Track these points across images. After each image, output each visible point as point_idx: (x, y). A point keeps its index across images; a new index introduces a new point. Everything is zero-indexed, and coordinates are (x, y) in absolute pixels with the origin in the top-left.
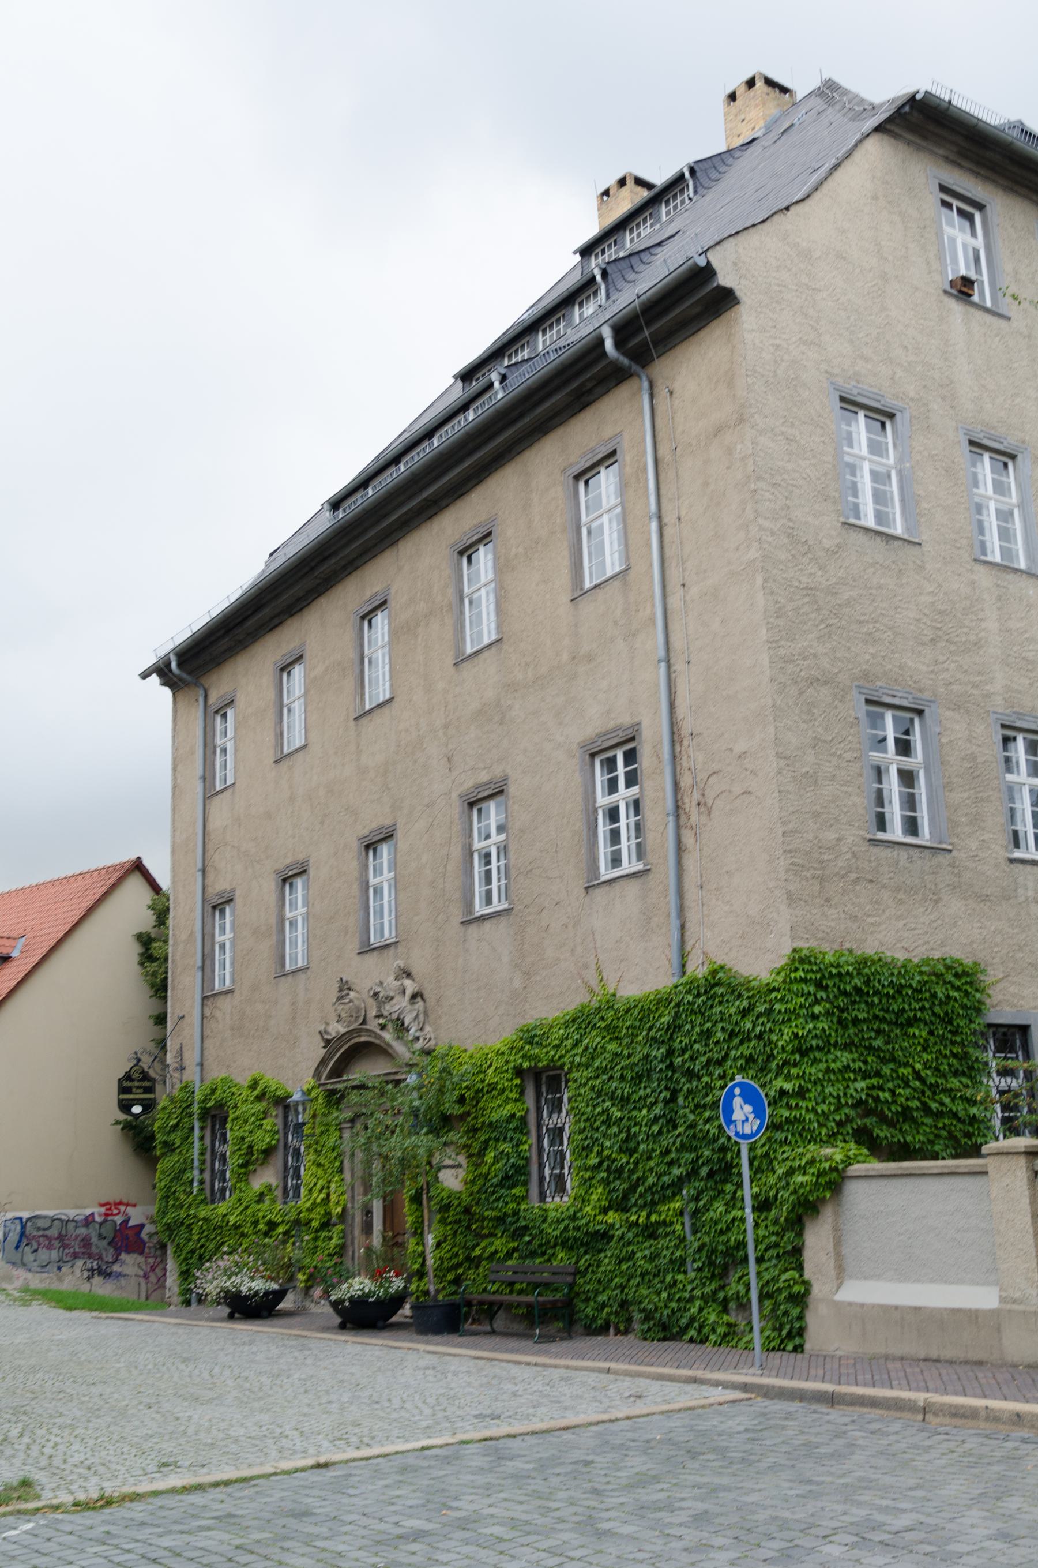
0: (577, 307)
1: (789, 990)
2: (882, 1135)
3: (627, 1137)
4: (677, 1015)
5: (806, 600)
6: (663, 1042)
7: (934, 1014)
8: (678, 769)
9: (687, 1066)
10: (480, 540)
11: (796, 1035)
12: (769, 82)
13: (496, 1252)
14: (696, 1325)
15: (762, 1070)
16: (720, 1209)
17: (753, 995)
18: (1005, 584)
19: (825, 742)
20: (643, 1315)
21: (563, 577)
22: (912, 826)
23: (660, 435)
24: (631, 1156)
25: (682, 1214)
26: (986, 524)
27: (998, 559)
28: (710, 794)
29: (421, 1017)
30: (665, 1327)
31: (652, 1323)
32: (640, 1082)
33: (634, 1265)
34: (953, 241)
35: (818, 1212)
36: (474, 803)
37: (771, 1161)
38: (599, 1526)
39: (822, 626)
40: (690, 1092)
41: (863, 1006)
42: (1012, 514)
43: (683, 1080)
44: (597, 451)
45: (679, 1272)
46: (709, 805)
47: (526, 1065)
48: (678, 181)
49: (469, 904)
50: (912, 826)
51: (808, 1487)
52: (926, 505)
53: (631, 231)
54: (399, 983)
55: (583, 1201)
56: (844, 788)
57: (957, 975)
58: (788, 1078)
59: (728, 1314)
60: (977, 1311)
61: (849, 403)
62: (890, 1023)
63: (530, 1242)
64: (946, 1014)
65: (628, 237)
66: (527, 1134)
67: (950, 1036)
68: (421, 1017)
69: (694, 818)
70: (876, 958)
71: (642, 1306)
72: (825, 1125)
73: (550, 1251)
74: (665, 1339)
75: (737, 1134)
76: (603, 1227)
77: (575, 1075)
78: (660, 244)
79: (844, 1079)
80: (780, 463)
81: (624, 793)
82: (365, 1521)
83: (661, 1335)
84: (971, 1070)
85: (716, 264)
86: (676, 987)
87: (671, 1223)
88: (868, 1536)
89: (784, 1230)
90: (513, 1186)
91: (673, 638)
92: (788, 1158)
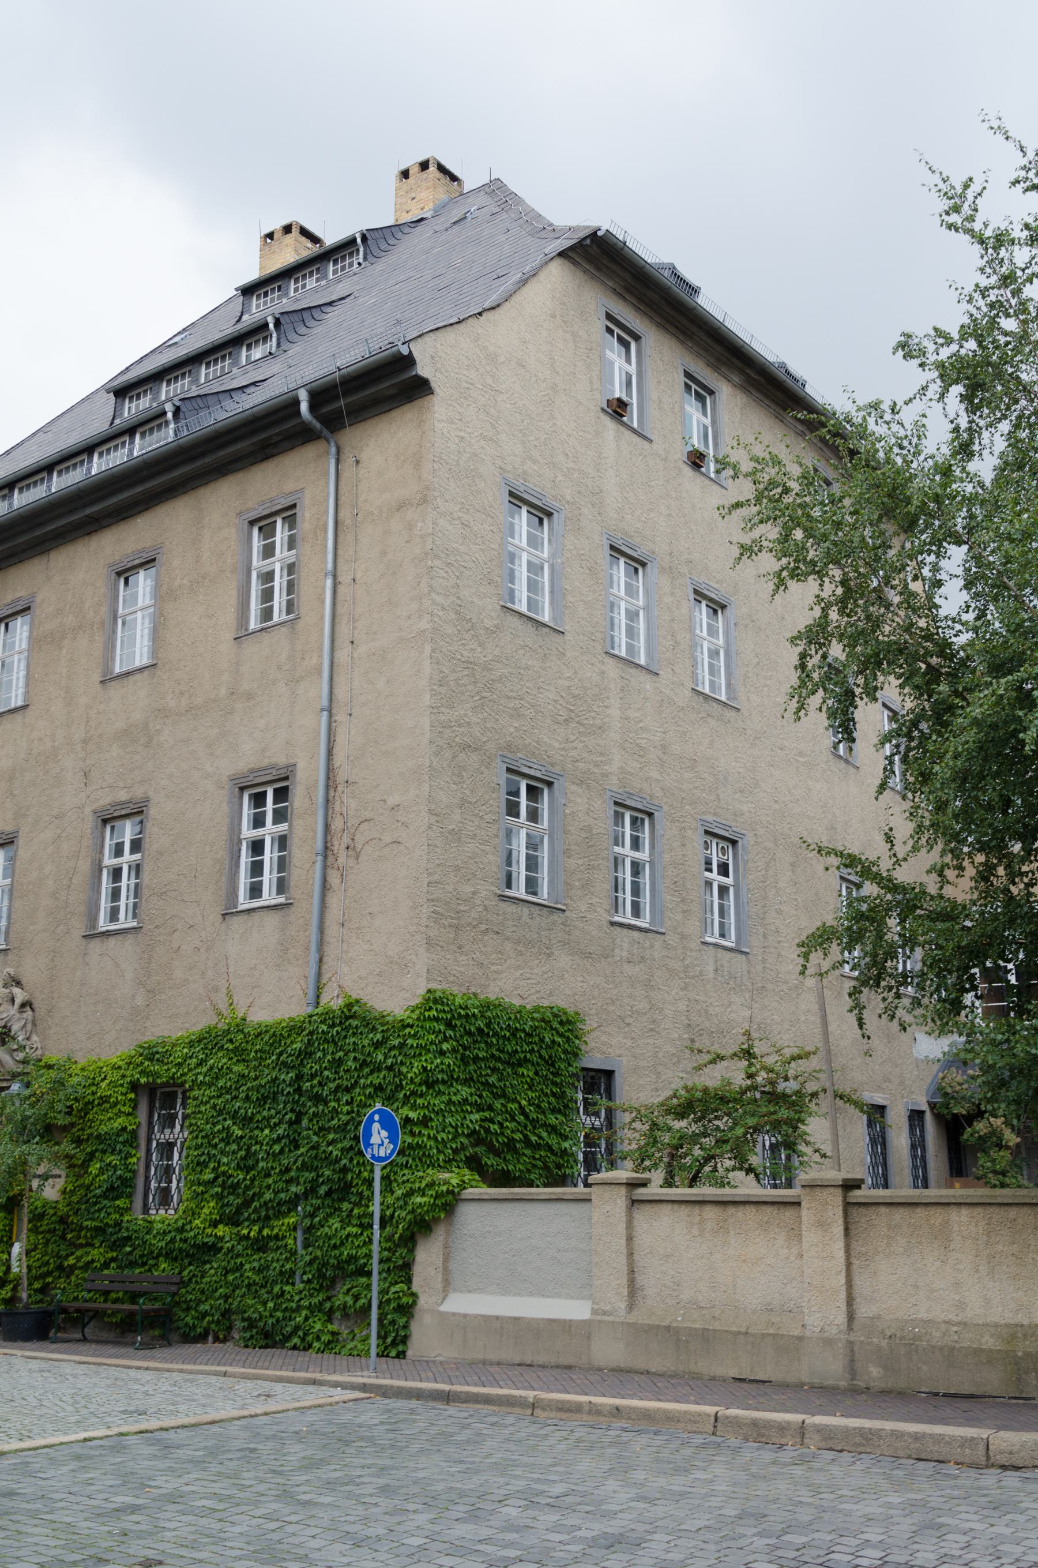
0: (244, 349)
1: (422, 1027)
2: (489, 1163)
3: (246, 1156)
4: (310, 1043)
5: (466, 673)
6: (294, 1066)
7: (541, 1056)
8: (330, 813)
9: (315, 1090)
10: (141, 565)
11: (425, 1069)
12: (441, 168)
13: (93, 1261)
14: (301, 1333)
15: (389, 1099)
16: (336, 1225)
17: (388, 1029)
18: (628, 677)
19: (470, 803)
20: (246, 1324)
21: (229, 617)
22: (532, 885)
23: (343, 499)
24: (248, 1173)
25: (295, 1229)
26: (517, 573)
27: (623, 653)
28: (360, 839)
29: (29, 1027)
30: (267, 1335)
31: (254, 1331)
32: (265, 1103)
33: (241, 1276)
34: (612, 364)
35: (431, 1231)
36: (107, 820)
37: (391, 1182)
38: (299, 1497)
39: (478, 698)
40: (315, 1115)
41: (483, 1045)
42: (637, 615)
43: (309, 1104)
44: (277, 502)
45: (288, 1283)
46: (358, 850)
47: (143, 1080)
48: (348, 246)
49: (93, 919)
50: (532, 885)
51: (465, 1466)
52: (571, 599)
53: (296, 281)
54: (8, 990)
55: (193, 1214)
56: (482, 847)
57: (561, 1023)
58: (414, 1107)
59: (332, 1324)
60: (570, 1321)
61: (516, 499)
62: (504, 1062)
63: (130, 1253)
64: (550, 1057)
65: (292, 286)
66: (136, 1148)
67: (551, 1077)
68: (29, 1027)
69: (342, 860)
70: (497, 1002)
71: (246, 1315)
72: (443, 1152)
73: (151, 1262)
74: (266, 1347)
75: (373, 1157)
76: (212, 1239)
77: (196, 1093)
78: (331, 304)
79: (462, 1111)
80: (455, 545)
81: (270, 830)
82: (72, 1498)
83: (263, 1343)
84: (565, 1108)
85: (416, 354)
86: (311, 1016)
87: (284, 1237)
88: (535, 1500)
89: (397, 1246)
90: (117, 1198)
91: (336, 691)
92: (408, 1180)
